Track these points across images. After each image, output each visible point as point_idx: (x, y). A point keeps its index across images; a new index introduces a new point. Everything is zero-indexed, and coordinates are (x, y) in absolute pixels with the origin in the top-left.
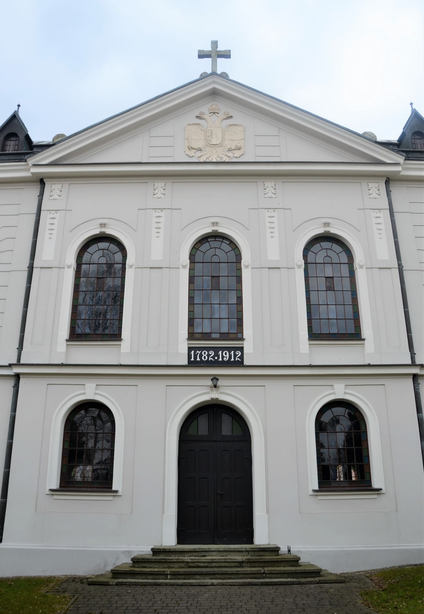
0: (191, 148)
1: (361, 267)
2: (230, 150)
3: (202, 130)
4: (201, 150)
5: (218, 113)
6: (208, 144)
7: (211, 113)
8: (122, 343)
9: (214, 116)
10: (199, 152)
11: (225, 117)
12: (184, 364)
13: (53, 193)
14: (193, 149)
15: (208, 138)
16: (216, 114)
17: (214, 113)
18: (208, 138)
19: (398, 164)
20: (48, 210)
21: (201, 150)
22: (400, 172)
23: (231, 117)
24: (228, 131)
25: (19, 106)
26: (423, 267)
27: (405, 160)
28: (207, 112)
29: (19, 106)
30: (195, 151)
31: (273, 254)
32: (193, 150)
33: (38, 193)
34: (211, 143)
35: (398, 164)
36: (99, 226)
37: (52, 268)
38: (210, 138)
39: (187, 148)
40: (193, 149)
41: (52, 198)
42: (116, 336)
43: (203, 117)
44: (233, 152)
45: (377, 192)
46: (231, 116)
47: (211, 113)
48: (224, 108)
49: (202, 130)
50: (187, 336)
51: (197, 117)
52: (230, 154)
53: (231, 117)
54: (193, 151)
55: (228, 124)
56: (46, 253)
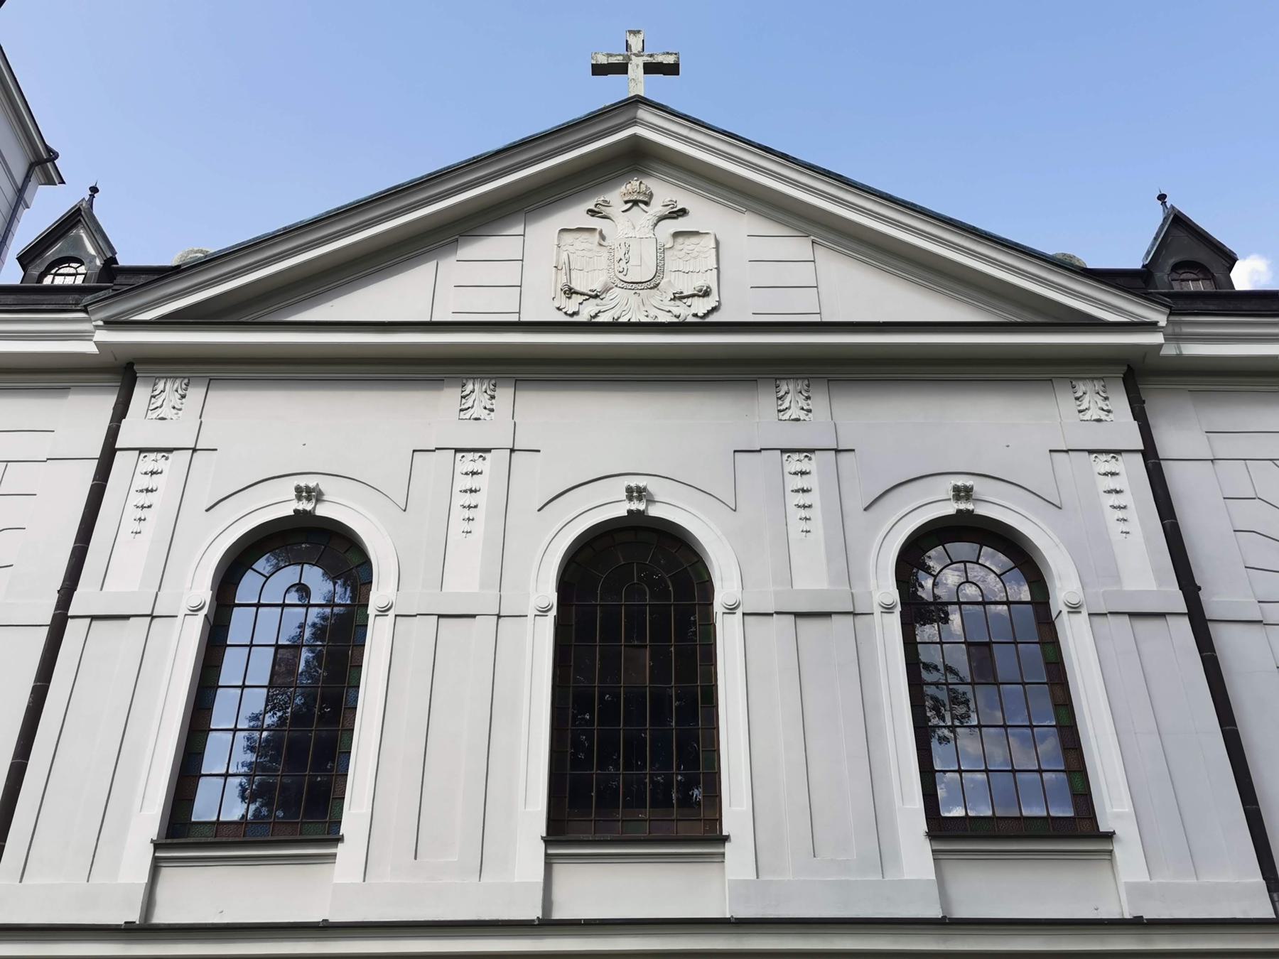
0: (570, 292)
1: (1075, 609)
2: (679, 297)
5: (646, 203)
6: (618, 282)
7: (626, 202)
8: (340, 850)
9: (635, 208)
11: (666, 211)
12: (118, 919)
13: (786, 405)
14: (577, 293)
16: (642, 205)
19: (1151, 326)
22: (1160, 346)
23: (683, 212)
25: (94, 190)
26: (1274, 613)
27: (1171, 314)
29: (94, 190)
31: (465, 582)
35: (1151, 326)
36: (624, 495)
37: (474, 616)
38: (623, 263)
40: (577, 293)
41: (786, 417)
42: (709, 835)
43: (606, 211)
44: (689, 301)
45: (1102, 404)
47: (626, 202)
48: (664, 192)
50: (542, 829)
51: (592, 213)
53: (683, 212)
56: (118, 576)
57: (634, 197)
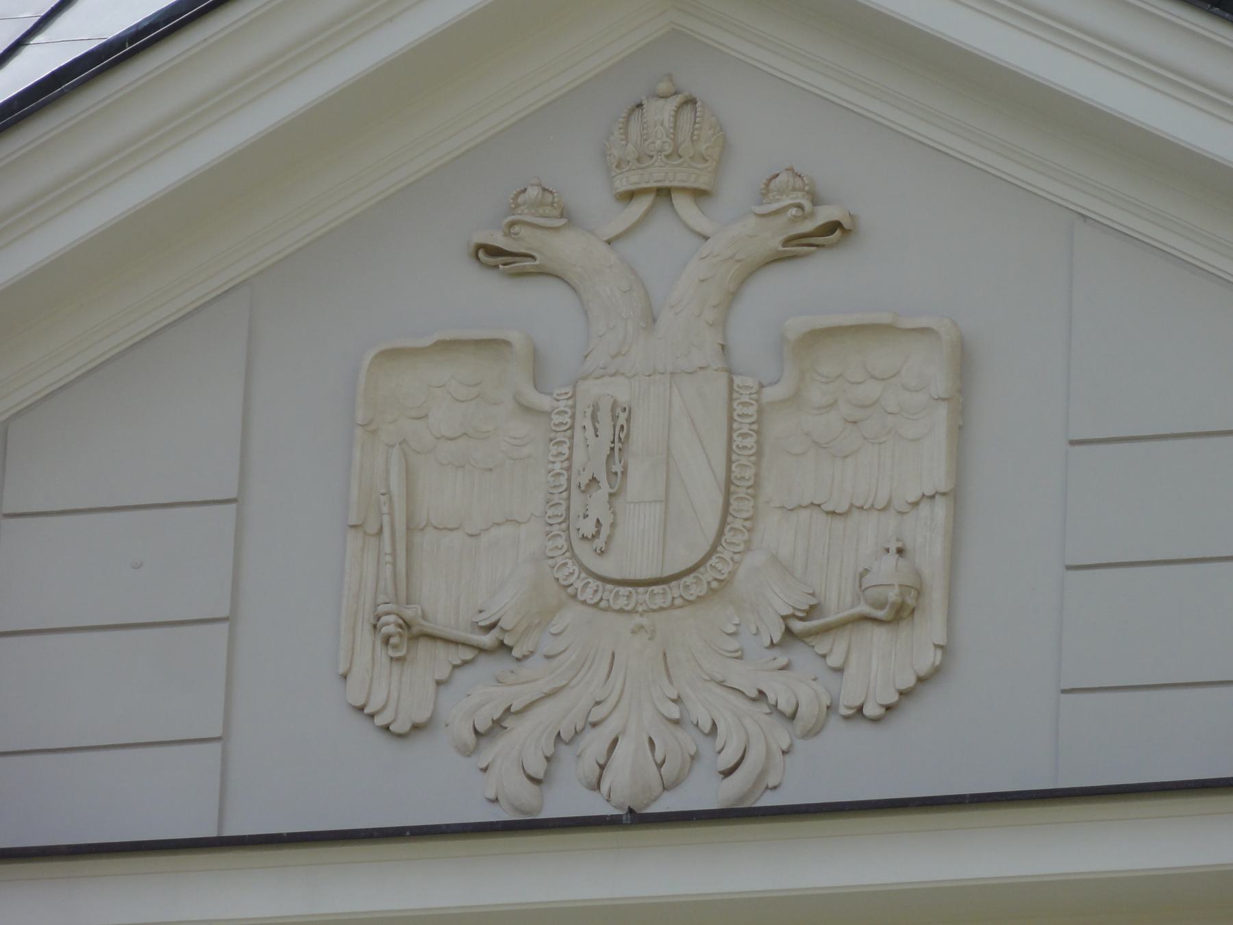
0: (408, 636)
2: (799, 631)
3: (528, 410)
4: (503, 647)
5: (699, 194)
10: (488, 667)
15: (577, 499)
16: (683, 204)
17: (664, 193)
18: (577, 499)
20: (636, 819)
21: (503, 647)
24: (795, 399)
28: (590, 192)
30: (447, 656)
32: (423, 647)
33: (943, 396)
34: (607, 567)
38: (598, 499)
39: (365, 636)
43: (565, 248)
46: (833, 227)
49: (528, 410)
52: (800, 685)
54: (439, 660)
55: (797, 325)
57: (657, 175)
